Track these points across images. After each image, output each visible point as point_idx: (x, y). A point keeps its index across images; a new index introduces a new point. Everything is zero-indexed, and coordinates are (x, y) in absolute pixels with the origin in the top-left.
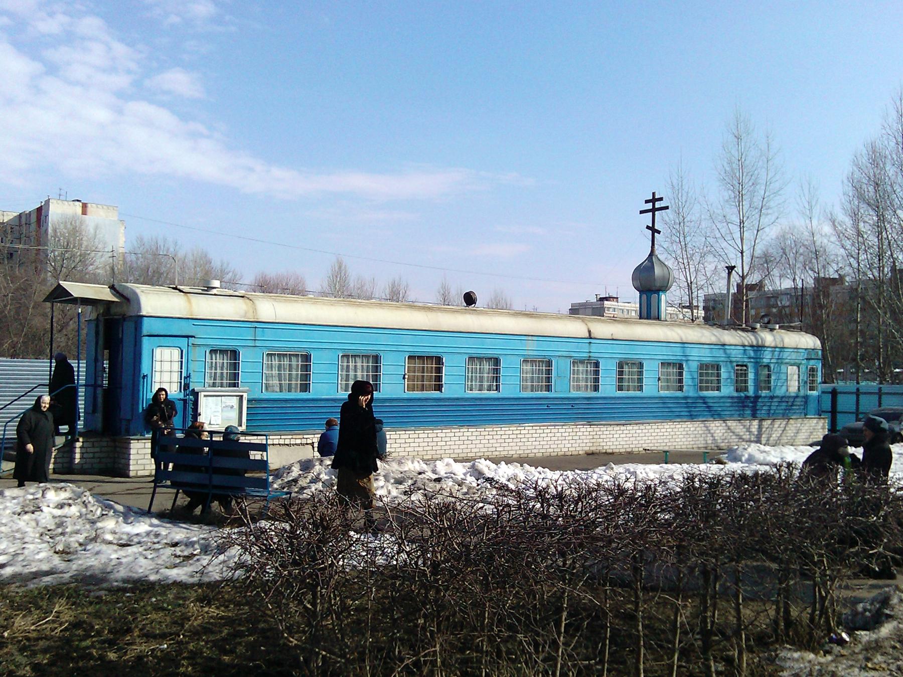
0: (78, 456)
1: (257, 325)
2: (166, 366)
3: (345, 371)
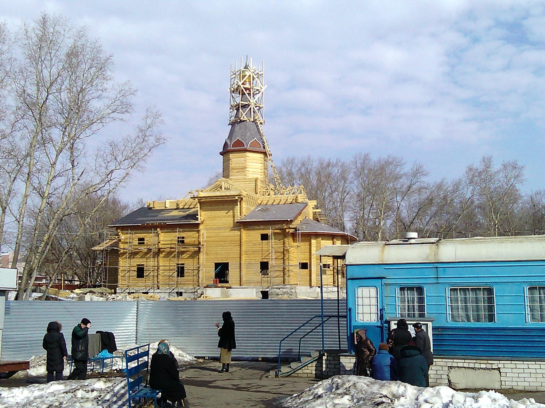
0: (324, 366)
1: (437, 265)
2: (366, 301)
3: (486, 302)
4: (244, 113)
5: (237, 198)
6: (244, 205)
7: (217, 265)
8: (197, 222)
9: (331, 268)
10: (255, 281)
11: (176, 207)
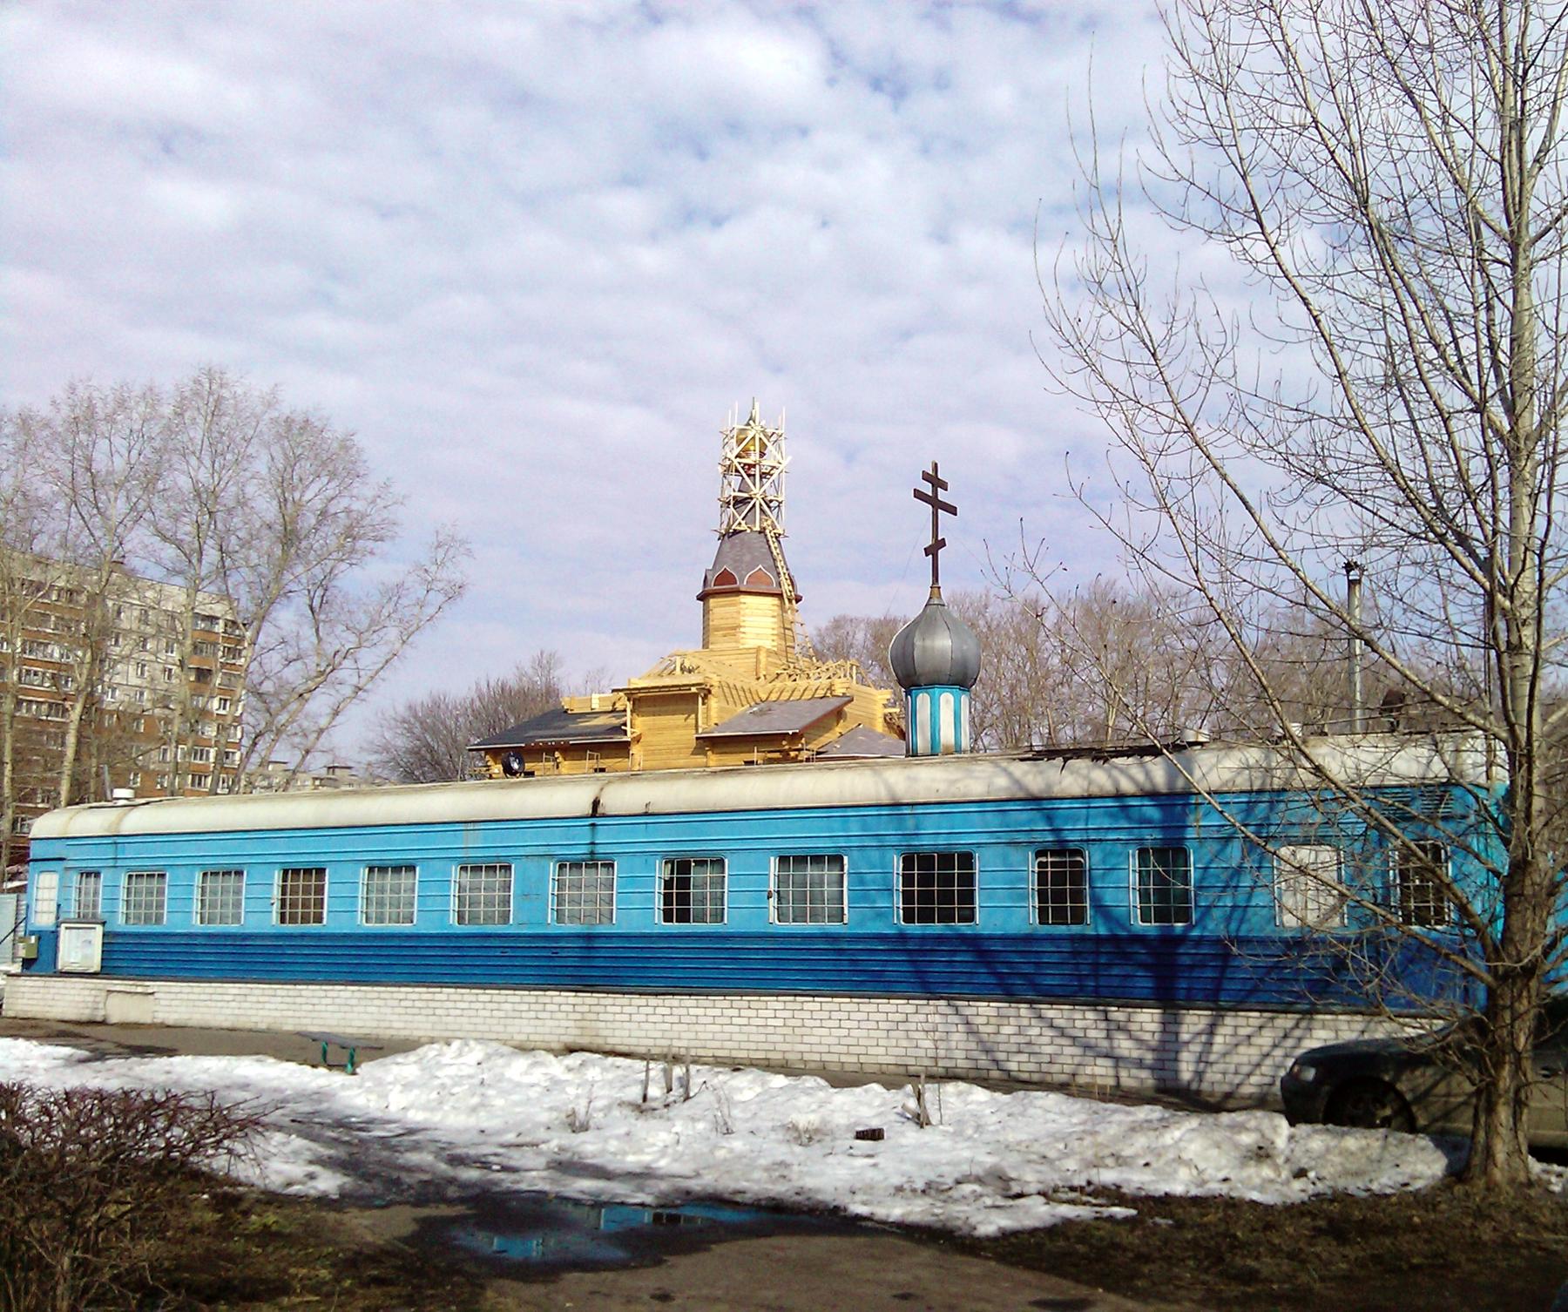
5: (694, 690)
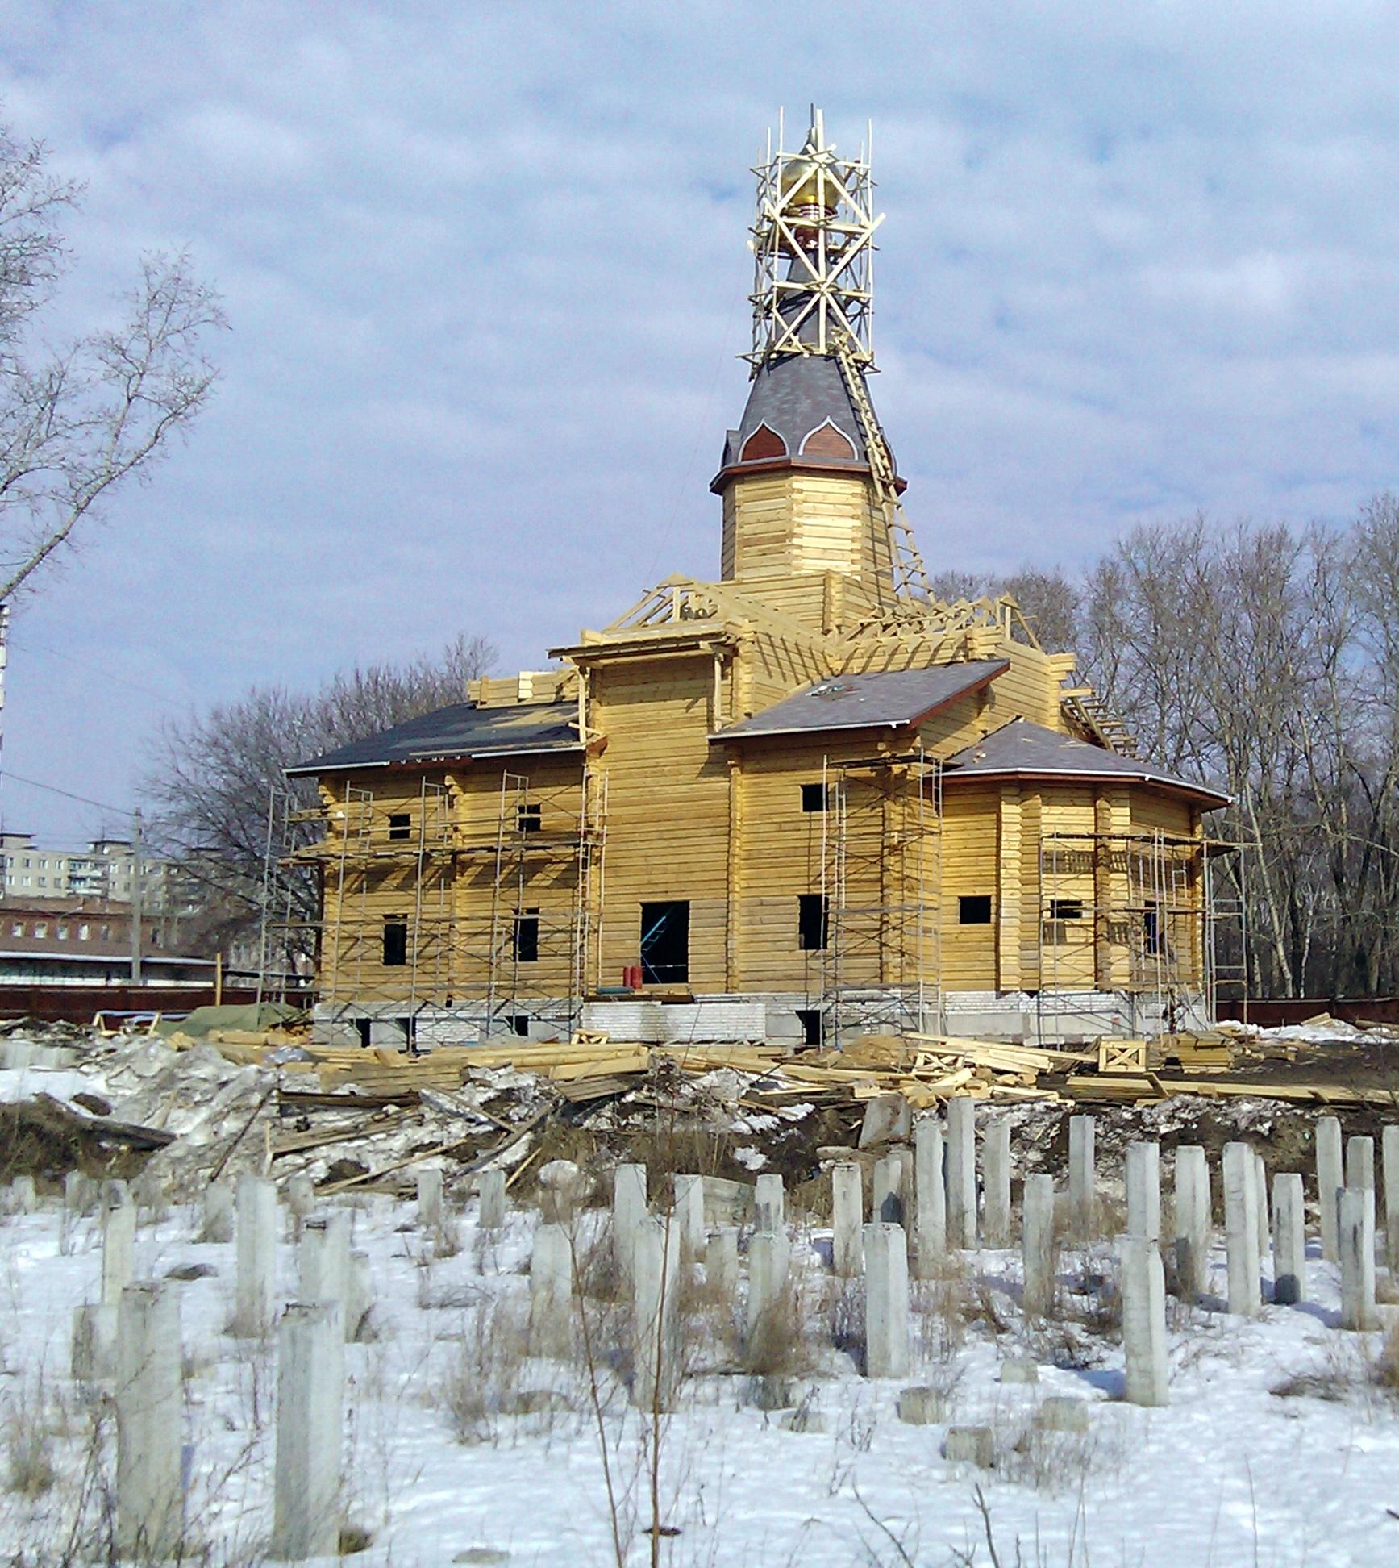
4: (789, 326)
6: (743, 672)
7: (651, 912)
8: (575, 747)
9: (1087, 917)
10: (778, 974)
11: (554, 696)
